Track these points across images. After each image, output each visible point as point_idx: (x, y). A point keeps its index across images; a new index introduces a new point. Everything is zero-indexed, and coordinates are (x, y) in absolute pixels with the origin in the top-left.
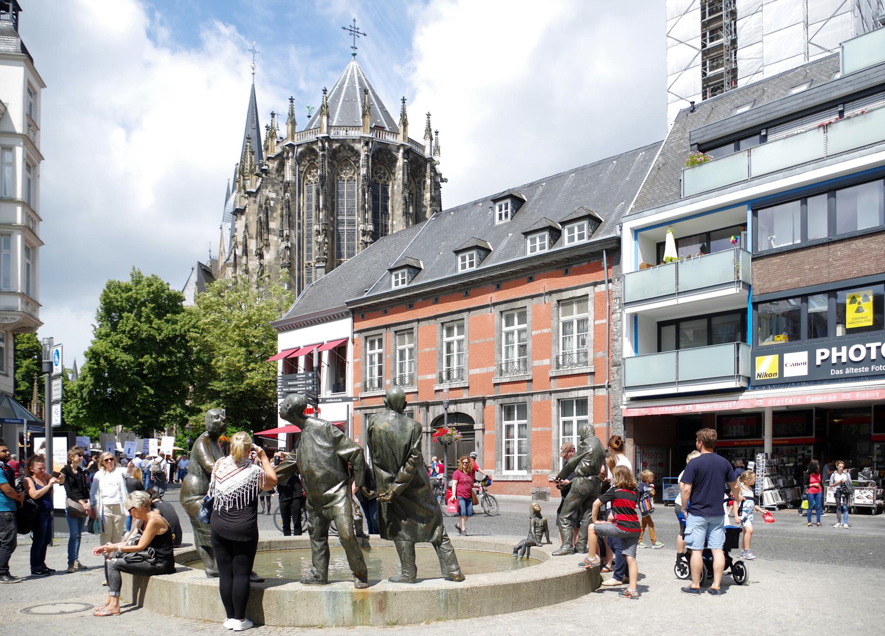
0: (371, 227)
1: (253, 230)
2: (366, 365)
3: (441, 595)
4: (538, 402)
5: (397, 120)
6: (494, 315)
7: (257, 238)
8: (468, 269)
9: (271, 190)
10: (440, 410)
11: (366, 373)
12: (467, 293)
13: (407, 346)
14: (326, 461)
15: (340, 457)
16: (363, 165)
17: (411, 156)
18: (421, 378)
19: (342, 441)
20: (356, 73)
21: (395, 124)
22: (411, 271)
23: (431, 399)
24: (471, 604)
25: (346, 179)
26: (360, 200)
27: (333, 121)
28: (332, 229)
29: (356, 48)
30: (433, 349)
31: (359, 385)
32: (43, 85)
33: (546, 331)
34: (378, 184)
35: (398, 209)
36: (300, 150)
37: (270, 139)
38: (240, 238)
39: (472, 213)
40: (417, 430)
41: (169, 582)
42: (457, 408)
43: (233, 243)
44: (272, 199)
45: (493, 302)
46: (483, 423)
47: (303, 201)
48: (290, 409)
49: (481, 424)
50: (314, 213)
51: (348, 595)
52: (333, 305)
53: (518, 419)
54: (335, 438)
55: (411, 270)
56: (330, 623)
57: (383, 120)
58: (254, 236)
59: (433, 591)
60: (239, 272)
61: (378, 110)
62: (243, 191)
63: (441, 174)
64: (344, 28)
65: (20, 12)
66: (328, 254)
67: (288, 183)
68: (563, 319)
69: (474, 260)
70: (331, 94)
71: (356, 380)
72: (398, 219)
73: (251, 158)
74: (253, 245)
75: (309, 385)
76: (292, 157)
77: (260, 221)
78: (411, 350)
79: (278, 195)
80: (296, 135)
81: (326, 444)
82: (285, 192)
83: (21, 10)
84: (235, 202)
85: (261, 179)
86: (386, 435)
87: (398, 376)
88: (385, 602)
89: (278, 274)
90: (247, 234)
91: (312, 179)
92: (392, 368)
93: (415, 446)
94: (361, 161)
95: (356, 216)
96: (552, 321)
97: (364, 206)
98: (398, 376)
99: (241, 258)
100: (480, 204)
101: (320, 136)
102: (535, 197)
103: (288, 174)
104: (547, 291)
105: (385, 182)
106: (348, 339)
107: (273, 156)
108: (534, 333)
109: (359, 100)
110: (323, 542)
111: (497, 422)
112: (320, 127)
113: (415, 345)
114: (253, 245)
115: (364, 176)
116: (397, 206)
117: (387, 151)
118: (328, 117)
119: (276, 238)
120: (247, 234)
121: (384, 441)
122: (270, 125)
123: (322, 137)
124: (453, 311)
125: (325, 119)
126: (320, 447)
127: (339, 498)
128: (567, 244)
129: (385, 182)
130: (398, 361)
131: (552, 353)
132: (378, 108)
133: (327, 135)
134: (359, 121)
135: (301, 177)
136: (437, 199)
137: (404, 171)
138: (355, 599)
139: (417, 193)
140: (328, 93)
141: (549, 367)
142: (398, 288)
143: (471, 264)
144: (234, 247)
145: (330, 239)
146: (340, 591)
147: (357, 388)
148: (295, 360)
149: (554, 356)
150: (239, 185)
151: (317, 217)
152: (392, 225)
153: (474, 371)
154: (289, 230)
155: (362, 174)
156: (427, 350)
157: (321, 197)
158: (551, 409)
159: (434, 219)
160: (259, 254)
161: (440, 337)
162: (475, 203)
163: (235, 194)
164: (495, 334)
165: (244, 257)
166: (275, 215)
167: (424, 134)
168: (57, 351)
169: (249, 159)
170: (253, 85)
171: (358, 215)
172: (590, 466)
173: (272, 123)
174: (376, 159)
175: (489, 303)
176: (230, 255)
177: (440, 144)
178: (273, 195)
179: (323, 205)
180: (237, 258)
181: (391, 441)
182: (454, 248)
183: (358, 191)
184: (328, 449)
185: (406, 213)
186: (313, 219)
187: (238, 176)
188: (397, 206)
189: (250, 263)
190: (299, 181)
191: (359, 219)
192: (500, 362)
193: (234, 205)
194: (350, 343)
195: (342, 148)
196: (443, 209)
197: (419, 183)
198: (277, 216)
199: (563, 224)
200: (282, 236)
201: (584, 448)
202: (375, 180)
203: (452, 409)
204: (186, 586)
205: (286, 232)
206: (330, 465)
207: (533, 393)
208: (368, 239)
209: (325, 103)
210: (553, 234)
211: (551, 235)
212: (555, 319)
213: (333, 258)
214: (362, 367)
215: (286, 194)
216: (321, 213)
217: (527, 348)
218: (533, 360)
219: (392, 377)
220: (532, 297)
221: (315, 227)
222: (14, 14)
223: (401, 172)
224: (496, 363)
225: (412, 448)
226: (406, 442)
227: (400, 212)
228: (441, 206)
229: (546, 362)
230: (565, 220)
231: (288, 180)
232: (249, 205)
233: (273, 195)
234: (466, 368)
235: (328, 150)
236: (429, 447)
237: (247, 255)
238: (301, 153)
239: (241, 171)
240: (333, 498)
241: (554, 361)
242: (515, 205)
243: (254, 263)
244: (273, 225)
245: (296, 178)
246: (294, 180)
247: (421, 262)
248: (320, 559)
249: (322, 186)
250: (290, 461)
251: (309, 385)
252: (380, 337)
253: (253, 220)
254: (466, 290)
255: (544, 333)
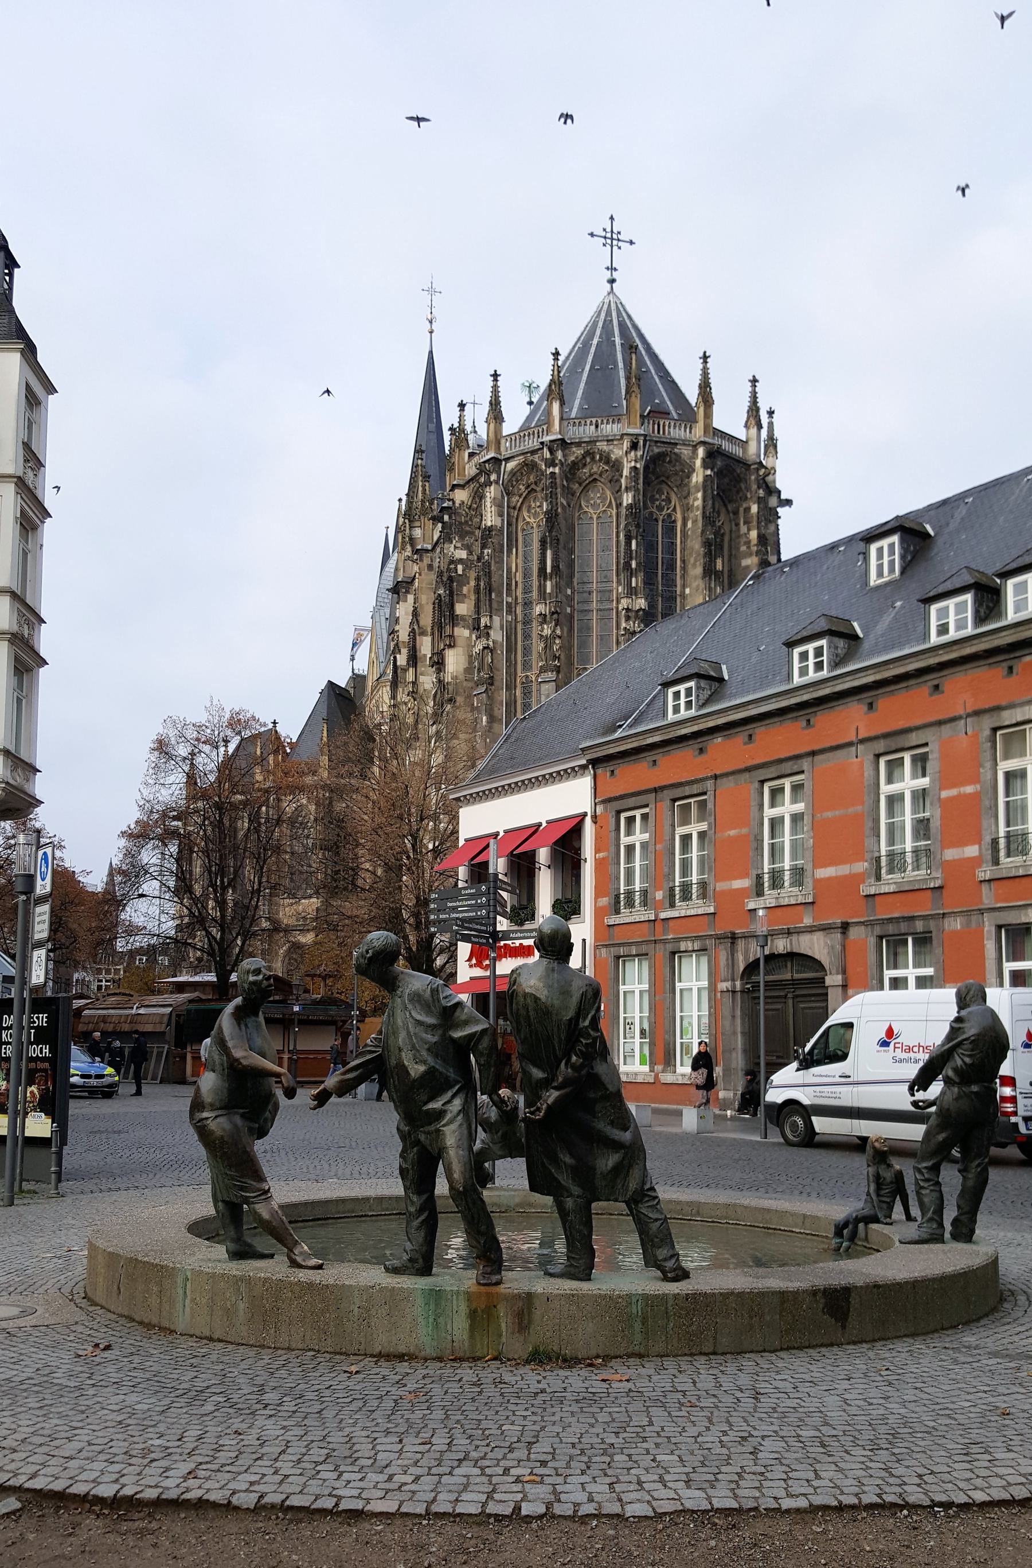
0: (641, 603)
1: (427, 619)
2: (619, 864)
3: (634, 1307)
4: (955, 932)
5: (692, 395)
6: (862, 764)
7: (433, 634)
8: (812, 675)
9: (459, 545)
10: (755, 952)
11: (618, 879)
12: (809, 721)
13: (694, 829)
14: (429, 1050)
15: (453, 1040)
16: (627, 488)
17: (719, 463)
18: (721, 886)
19: (458, 1013)
20: (614, 314)
21: (689, 404)
22: (703, 685)
23: (741, 928)
24: (694, 1328)
25: (595, 517)
26: (622, 554)
27: (571, 410)
28: (569, 610)
29: (615, 269)
30: (744, 831)
31: (604, 901)
32: (51, 389)
33: (969, 789)
34: (656, 520)
35: (694, 566)
36: (511, 465)
37: (457, 450)
38: (404, 635)
39: (825, 567)
40: (590, 994)
41: (162, 1267)
42: (791, 944)
43: (392, 644)
44: (460, 561)
45: (860, 737)
46: (844, 972)
47: (514, 562)
48: (370, 959)
49: (840, 977)
50: (535, 583)
51: (461, 1297)
52: (559, 753)
53: (915, 967)
54: (445, 1008)
55: (703, 683)
56: (428, 1351)
57: (666, 399)
58: (429, 630)
59: (620, 1297)
60: (402, 696)
61: (657, 380)
62: (409, 548)
63: (779, 492)
64: (592, 235)
65: (16, 270)
66: (562, 657)
67: (490, 529)
68: (1005, 765)
69: (825, 658)
70: (567, 358)
71: (598, 893)
72: (695, 585)
73: (424, 486)
74: (425, 646)
75: (481, 906)
76: (497, 482)
77: (439, 602)
78: (702, 835)
79: (470, 553)
80: (503, 441)
81: (431, 1020)
82: (484, 546)
83: (19, 267)
84: (397, 569)
85: (440, 525)
86: (535, 1002)
87: (677, 884)
88: (530, 1313)
89: (469, 697)
90: (416, 627)
91: (532, 520)
92: (666, 870)
93: (587, 1023)
94: (623, 481)
95: (615, 585)
96: (981, 770)
97: (627, 564)
98: (677, 884)
99: (405, 670)
100: (842, 549)
101: (547, 439)
102: (952, 526)
103: (489, 515)
104: (969, 710)
105: (669, 515)
106: (585, 815)
107: (462, 482)
108: (944, 794)
109: (621, 365)
110: (425, 1197)
111: (873, 970)
112: (548, 420)
113: (709, 825)
114: (425, 646)
115: (630, 507)
116: (692, 560)
117: (673, 456)
118: (562, 404)
119: (466, 633)
120: (416, 627)
121: (532, 1013)
122: (456, 425)
123: (551, 441)
124: (782, 756)
125: (556, 406)
126: (419, 1023)
127: (448, 1116)
128: (1011, 615)
129: (669, 515)
130: (678, 857)
131: (983, 832)
132: (656, 377)
133: (560, 437)
134: (620, 405)
135: (512, 517)
136: (771, 540)
137: (705, 492)
138: (474, 1306)
139: (731, 531)
140: (561, 358)
141: (977, 861)
142: (678, 717)
143: (819, 666)
144: (393, 652)
145: (565, 629)
146: (448, 1288)
147: (601, 908)
148: (530, 857)
149: (987, 839)
150: (403, 538)
151: (542, 589)
152: (683, 596)
153: (823, 873)
154: (491, 617)
155: (625, 504)
156: (732, 833)
157: (549, 553)
158: (983, 946)
159: (751, 582)
160: (438, 663)
161: (757, 808)
162: (833, 547)
163: (396, 554)
164: (866, 798)
165: (411, 669)
166: (465, 590)
167: (745, 419)
168: (45, 854)
169: (420, 489)
170: (431, 353)
171: (619, 582)
172: (972, 1065)
173: (459, 422)
174: (653, 473)
175: (854, 739)
176: (386, 667)
177: (777, 434)
178: (463, 554)
179: (552, 567)
180: (399, 671)
181: (544, 1011)
182: (784, 639)
183: (618, 536)
184: (432, 1028)
185: (709, 571)
186: (535, 594)
187: (401, 520)
188: (692, 560)
189: (422, 679)
190: (509, 524)
191: (620, 589)
192: (877, 854)
193: (395, 575)
194: (588, 820)
195: (588, 460)
196: (784, 558)
197: (736, 513)
198: (469, 591)
199: (1006, 575)
200: (478, 629)
201: (960, 1028)
202: (651, 513)
203: (781, 945)
204: (189, 1274)
205: (484, 621)
206: (436, 1056)
207: (944, 914)
208: (635, 625)
209: (556, 378)
210: (982, 597)
211: (978, 603)
212: (988, 765)
213: (570, 663)
214: (611, 869)
215: (486, 551)
216: (549, 584)
217: (931, 825)
218: (943, 848)
219: (666, 887)
220: (940, 723)
221: (539, 609)
222: (6, 274)
223: (700, 495)
224: (867, 856)
225: (581, 1025)
226: (570, 1014)
227: (699, 570)
228: (779, 553)
229: (972, 851)
230: (1008, 568)
231: (489, 524)
232: (420, 574)
233: (463, 554)
234: (809, 867)
235: (562, 464)
236: (738, 1021)
237: (415, 666)
238: (513, 473)
239: (409, 515)
240: (440, 1114)
241: (987, 850)
242: (908, 546)
243: (428, 681)
244: (462, 609)
245: (503, 520)
246: (499, 525)
247: (724, 667)
248: (418, 1228)
249: (550, 531)
250: (374, 1049)
251: (481, 906)
252: (646, 810)
253: (427, 600)
254: (808, 717)
255: (966, 795)
